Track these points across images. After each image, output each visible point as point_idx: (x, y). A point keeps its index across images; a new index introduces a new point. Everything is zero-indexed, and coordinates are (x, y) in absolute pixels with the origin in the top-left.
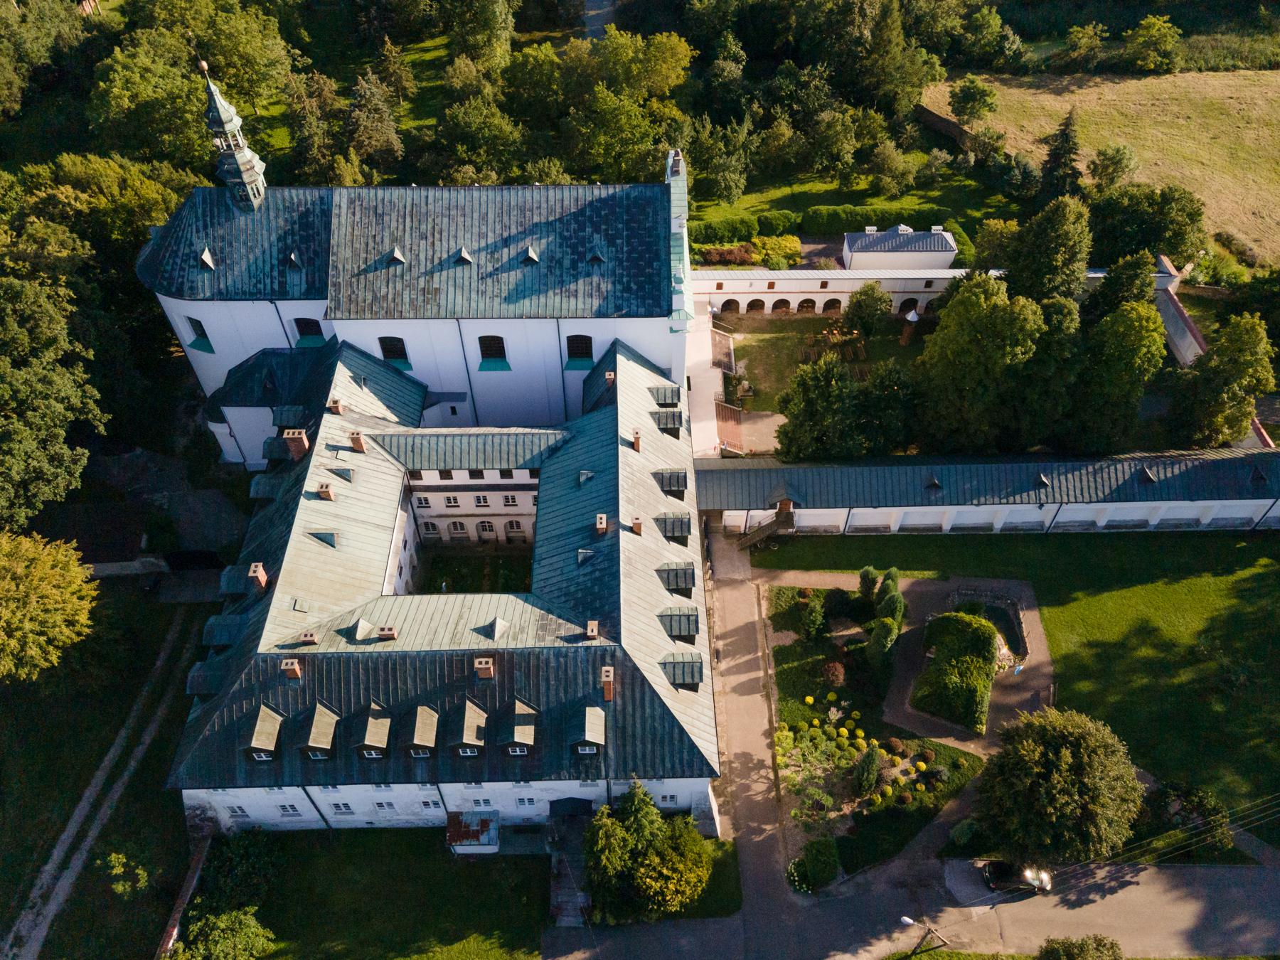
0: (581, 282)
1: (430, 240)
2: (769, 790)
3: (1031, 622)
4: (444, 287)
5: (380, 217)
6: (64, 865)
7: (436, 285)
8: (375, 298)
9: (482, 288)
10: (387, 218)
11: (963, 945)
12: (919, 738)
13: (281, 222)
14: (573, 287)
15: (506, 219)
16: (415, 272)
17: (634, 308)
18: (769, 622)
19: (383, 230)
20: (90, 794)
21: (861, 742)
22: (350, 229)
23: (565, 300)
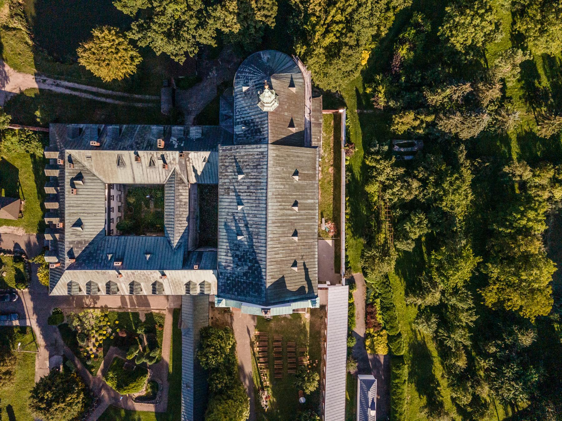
0: (231, 258)
1: (247, 191)
2: (86, 305)
3: (150, 408)
4: (230, 197)
5: (256, 167)
6: (67, 88)
7: (231, 194)
8: (227, 166)
9: (230, 214)
10: (255, 170)
11: (38, 356)
12: (104, 356)
13: (257, 120)
14: (229, 254)
15: (254, 226)
17: (221, 281)
18: (149, 312)
19: (251, 169)
20: (89, 88)
22: (251, 153)
23: (225, 250)
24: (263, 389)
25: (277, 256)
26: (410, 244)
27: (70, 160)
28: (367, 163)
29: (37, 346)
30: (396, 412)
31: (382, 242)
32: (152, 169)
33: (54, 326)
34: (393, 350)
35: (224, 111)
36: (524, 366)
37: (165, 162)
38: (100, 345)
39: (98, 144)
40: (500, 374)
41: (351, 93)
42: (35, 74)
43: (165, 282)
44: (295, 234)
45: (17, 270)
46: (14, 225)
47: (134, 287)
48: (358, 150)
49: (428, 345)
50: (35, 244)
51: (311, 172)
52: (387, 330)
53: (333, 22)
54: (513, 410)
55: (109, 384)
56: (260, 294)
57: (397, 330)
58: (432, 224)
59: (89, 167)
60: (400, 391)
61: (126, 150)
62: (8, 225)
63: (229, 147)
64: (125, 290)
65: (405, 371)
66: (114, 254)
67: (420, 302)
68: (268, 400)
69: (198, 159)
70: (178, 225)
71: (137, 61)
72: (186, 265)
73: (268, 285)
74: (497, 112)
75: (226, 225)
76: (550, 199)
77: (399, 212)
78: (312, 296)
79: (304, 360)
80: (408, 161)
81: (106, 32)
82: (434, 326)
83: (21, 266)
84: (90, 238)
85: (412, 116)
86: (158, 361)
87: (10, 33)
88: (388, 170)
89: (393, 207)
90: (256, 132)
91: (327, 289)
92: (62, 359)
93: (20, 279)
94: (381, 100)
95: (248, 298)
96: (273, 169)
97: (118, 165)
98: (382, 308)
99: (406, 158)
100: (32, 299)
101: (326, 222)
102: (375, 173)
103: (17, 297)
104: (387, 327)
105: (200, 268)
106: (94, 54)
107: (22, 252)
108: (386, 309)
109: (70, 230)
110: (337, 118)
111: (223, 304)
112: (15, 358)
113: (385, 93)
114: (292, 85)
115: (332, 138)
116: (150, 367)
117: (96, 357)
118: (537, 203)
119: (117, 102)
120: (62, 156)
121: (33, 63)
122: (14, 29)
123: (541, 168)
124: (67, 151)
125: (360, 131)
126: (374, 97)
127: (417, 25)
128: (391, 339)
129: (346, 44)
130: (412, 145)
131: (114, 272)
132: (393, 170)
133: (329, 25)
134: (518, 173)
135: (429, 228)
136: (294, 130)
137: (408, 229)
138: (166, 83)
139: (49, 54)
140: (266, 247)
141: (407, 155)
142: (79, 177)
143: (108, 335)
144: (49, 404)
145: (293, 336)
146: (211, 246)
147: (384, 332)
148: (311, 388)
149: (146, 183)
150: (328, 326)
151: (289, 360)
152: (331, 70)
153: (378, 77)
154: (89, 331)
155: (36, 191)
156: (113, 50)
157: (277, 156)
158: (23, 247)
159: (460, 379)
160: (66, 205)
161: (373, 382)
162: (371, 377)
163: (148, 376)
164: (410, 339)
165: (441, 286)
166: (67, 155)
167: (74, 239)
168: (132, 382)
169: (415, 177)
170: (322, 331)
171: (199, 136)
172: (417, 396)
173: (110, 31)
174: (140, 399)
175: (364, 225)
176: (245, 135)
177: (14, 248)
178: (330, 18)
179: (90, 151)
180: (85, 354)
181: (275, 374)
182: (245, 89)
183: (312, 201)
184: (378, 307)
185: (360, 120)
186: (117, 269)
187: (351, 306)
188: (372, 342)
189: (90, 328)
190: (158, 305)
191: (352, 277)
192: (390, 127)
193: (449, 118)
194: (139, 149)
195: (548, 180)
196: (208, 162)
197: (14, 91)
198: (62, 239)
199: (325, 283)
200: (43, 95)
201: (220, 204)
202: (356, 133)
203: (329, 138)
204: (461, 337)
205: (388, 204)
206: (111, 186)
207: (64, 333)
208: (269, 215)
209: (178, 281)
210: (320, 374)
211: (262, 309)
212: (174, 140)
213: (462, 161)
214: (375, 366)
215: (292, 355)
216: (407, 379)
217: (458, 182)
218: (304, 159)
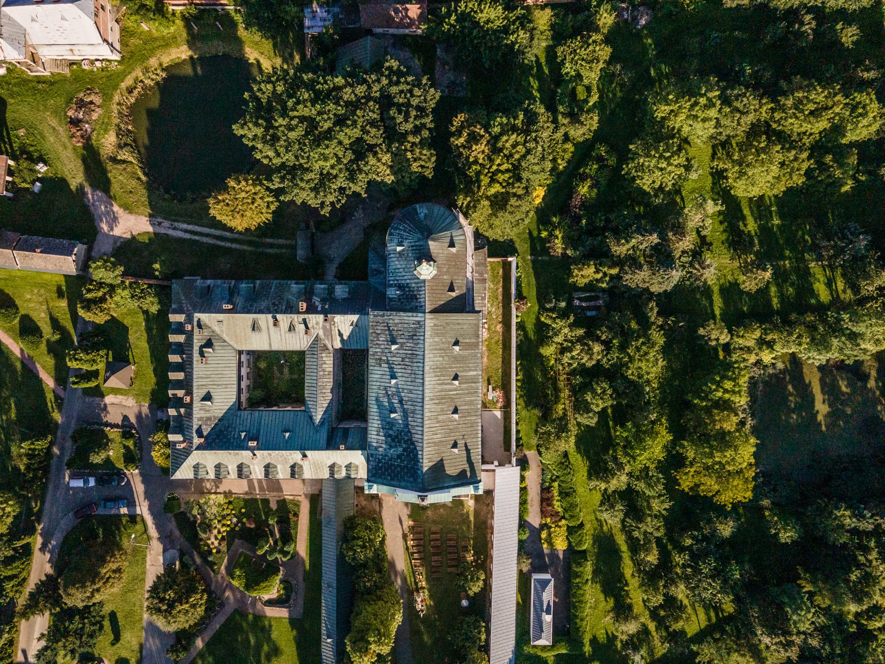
0: (383, 438)
3: (282, 613)
5: (411, 337)
6: (186, 231)
8: (379, 334)
12: (228, 550)
13: (413, 285)
14: (381, 434)
15: (410, 403)
16: (389, 355)
21: (224, 529)
24: (417, 590)
25: (435, 437)
26: (592, 418)
27: (200, 326)
28: (543, 319)
29: (149, 538)
30: (576, 617)
31: (561, 413)
32: (292, 334)
33: (170, 515)
34: (574, 544)
35: (373, 265)
36: (724, 560)
37: (307, 327)
38: (223, 538)
39: (230, 307)
40: (697, 571)
41: (523, 236)
42: (150, 216)
43: (305, 464)
44: (455, 411)
45: (125, 447)
46: (122, 394)
47: (270, 470)
48: (532, 305)
49: (616, 538)
50: (147, 415)
51: (473, 341)
52: (566, 519)
53: (498, 171)
54: (717, 615)
55: (235, 583)
56: (415, 480)
57: (578, 520)
58: (618, 394)
59: (218, 332)
60: (581, 592)
61: (263, 313)
62: (116, 394)
63: (381, 313)
64: (258, 473)
65: (588, 568)
66: (248, 432)
67: (603, 486)
68: (424, 604)
69: (345, 323)
70: (321, 397)
71: (273, 207)
72: (331, 445)
73: (425, 469)
74: (691, 265)
75: (377, 400)
76: (758, 363)
77: (578, 380)
78: (474, 480)
79: (467, 556)
80: (591, 317)
81: (243, 183)
82: (621, 515)
83: (130, 443)
84: (220, 414)
85: (592, 269)
86: (292, 557)
87: (119, 167)
88: (566, 330)
89: (573, 373)
90: (412, 299)
91: (494, 471)
92: (177, 555)
93: (129, 458)
94: (558, 246)
95: (403, 484)
96: (431, 340)
97: (253, 329)
98: (560, 494)
99: (589, 314)
100: (143, 482)
101: (493, 390)
102: (551, 333)
103: (126, 480)
104: (567, 516)
105: (347, 449)
106: (228, 205)
107: (131, 426)
108: (565, 494)
109: (199, 405)
110: (507, 266)
111: (375, 489)
112: (126, 553)
113: (563, 238)
114: (452, 245)
115: (501, 289)
116: (284, 564)
117: (218, 552)
118: (737, 371)
119: (245, 247)
120: (189, 319)
121: (146, 203)
122: (124, 162)
123: (745, 327)
124: (196, 315)
125: (533, 281)
126: (549, 242)
127: (600, 159)
128: (571, 530)
129: (515, 195)
130: (596, 298)
131: (249, 453)
132: (571, 331)
133: (494, 174)
134: (713, 337)
135: (613, 399)
136: (454, 294)
137: (589, 400)
138: (303, 225)
139: (167, 192)
140: (423, 427)
141: (590, 310)
142: (209, 344)
143: (233, 526)
144: (171, 606)
145: (454, 527)
146: (357, 419)
147: (564, 522)
148: (475, 588)
149: (284, 349)
150: (495, 516)
151: (450, 556)
152: (497, 222)
153: (554, 219)
154: (210, 520)
155: (149, 354)
156: (250, 201)
157: (435, 325)
158: (133, 420)
159: (651, 577)
160: (195, 376)
161: (549, 581)
162: (547, 576)
163: (280, 576)
164: (595, 529)
165: (628, 469)
166: (196, 320)
167: (205, 415)
168: (263, 581)
169: (598, 339)
170: (489, 521)
171: (346, 296)
172: (603, 599)
173: (246, 180)
174: (270, 603)
175: (538, 393)
176: (399, 299)
177: (123, 421)
178: (495, 167)
179: (222, 315)
180: (206, 548)
181: (433, 572)
182: (399, 249)
183: (475, 373)
184: (556, 493)
185: (533, 268)
186: (252, 449)
187: (523, 490)
188: (549, 534)
189: (213, 517)
190: (293, 490)
191: (525, 456)
192: (568, 279)
193: (634, 273)
194: (277, 313)
195: (754, 341)
196: (356, 326)
197: (124, 236)
198: (189, 415)
199: (492, 463)
200: (158, 238)
201: (370, 376)
202: (529, 284)
203: (497, 290)
204: (652, 527)
205: (567, 369)
206: (240, 353)
207: (182, 525)
208: (426, 391)
209: (319, 463)
210: (486, 574)
211: (419, 496)
212: (316, 300)
213: (653, 319)
214: (552, 563)
215: (454, 548)
216: (590, 577)
217: (644, 348)
218: (465, 327)
